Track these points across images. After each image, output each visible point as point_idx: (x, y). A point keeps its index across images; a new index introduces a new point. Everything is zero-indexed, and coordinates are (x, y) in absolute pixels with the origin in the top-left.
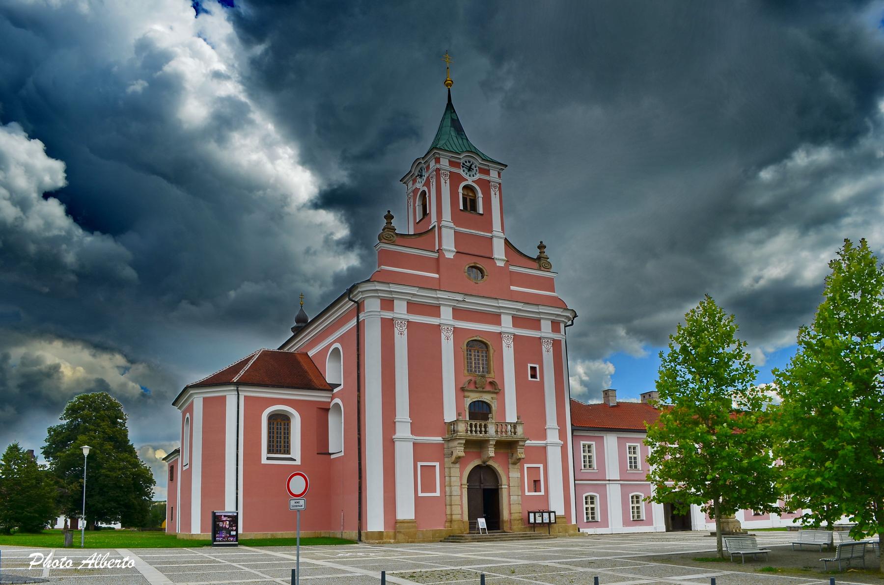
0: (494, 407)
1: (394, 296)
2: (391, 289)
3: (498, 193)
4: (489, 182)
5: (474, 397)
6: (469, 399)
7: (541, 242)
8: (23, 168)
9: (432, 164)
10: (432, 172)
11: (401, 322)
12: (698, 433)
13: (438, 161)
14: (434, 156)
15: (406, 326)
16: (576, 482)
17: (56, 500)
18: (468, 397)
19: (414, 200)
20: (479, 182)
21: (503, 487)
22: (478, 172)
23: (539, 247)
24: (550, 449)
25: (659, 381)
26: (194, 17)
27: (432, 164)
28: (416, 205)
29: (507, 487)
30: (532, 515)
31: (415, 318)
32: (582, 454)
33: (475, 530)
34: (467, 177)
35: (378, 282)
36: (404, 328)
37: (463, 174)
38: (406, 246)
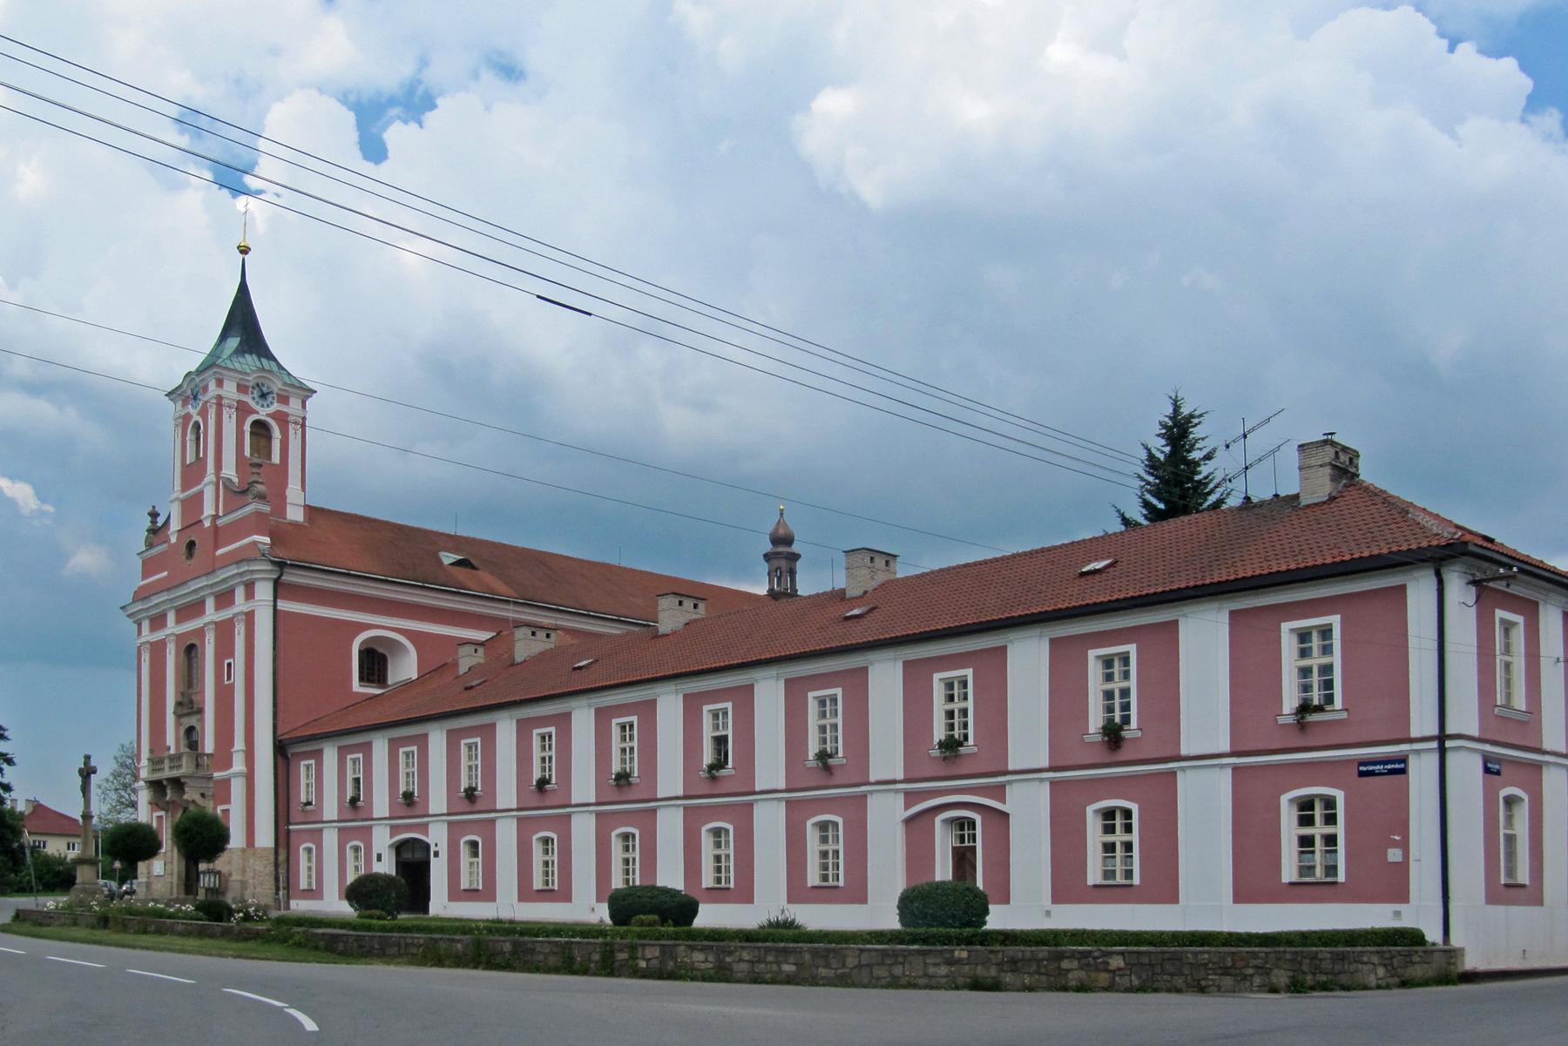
1: (231, 583)
3: (299, 432)
4: (287, 415)
7: (154, 507)
8: (1329, 467)
9: (212, 387)
10: (211, 398)
12: (251, 906)
13: (220, 383)
19: (183, 430)
20: (275, 416)
22: (275, 401)
23: (150, 514)
24: (233, 781)
25: (95, 820)
26: (1142, 441)
27: (212, 387)
28: (188, 438)
33: (969, 830)
34: (257, 408)
35: (154, 594)
37: (252, 404)
38: (1001, 438)
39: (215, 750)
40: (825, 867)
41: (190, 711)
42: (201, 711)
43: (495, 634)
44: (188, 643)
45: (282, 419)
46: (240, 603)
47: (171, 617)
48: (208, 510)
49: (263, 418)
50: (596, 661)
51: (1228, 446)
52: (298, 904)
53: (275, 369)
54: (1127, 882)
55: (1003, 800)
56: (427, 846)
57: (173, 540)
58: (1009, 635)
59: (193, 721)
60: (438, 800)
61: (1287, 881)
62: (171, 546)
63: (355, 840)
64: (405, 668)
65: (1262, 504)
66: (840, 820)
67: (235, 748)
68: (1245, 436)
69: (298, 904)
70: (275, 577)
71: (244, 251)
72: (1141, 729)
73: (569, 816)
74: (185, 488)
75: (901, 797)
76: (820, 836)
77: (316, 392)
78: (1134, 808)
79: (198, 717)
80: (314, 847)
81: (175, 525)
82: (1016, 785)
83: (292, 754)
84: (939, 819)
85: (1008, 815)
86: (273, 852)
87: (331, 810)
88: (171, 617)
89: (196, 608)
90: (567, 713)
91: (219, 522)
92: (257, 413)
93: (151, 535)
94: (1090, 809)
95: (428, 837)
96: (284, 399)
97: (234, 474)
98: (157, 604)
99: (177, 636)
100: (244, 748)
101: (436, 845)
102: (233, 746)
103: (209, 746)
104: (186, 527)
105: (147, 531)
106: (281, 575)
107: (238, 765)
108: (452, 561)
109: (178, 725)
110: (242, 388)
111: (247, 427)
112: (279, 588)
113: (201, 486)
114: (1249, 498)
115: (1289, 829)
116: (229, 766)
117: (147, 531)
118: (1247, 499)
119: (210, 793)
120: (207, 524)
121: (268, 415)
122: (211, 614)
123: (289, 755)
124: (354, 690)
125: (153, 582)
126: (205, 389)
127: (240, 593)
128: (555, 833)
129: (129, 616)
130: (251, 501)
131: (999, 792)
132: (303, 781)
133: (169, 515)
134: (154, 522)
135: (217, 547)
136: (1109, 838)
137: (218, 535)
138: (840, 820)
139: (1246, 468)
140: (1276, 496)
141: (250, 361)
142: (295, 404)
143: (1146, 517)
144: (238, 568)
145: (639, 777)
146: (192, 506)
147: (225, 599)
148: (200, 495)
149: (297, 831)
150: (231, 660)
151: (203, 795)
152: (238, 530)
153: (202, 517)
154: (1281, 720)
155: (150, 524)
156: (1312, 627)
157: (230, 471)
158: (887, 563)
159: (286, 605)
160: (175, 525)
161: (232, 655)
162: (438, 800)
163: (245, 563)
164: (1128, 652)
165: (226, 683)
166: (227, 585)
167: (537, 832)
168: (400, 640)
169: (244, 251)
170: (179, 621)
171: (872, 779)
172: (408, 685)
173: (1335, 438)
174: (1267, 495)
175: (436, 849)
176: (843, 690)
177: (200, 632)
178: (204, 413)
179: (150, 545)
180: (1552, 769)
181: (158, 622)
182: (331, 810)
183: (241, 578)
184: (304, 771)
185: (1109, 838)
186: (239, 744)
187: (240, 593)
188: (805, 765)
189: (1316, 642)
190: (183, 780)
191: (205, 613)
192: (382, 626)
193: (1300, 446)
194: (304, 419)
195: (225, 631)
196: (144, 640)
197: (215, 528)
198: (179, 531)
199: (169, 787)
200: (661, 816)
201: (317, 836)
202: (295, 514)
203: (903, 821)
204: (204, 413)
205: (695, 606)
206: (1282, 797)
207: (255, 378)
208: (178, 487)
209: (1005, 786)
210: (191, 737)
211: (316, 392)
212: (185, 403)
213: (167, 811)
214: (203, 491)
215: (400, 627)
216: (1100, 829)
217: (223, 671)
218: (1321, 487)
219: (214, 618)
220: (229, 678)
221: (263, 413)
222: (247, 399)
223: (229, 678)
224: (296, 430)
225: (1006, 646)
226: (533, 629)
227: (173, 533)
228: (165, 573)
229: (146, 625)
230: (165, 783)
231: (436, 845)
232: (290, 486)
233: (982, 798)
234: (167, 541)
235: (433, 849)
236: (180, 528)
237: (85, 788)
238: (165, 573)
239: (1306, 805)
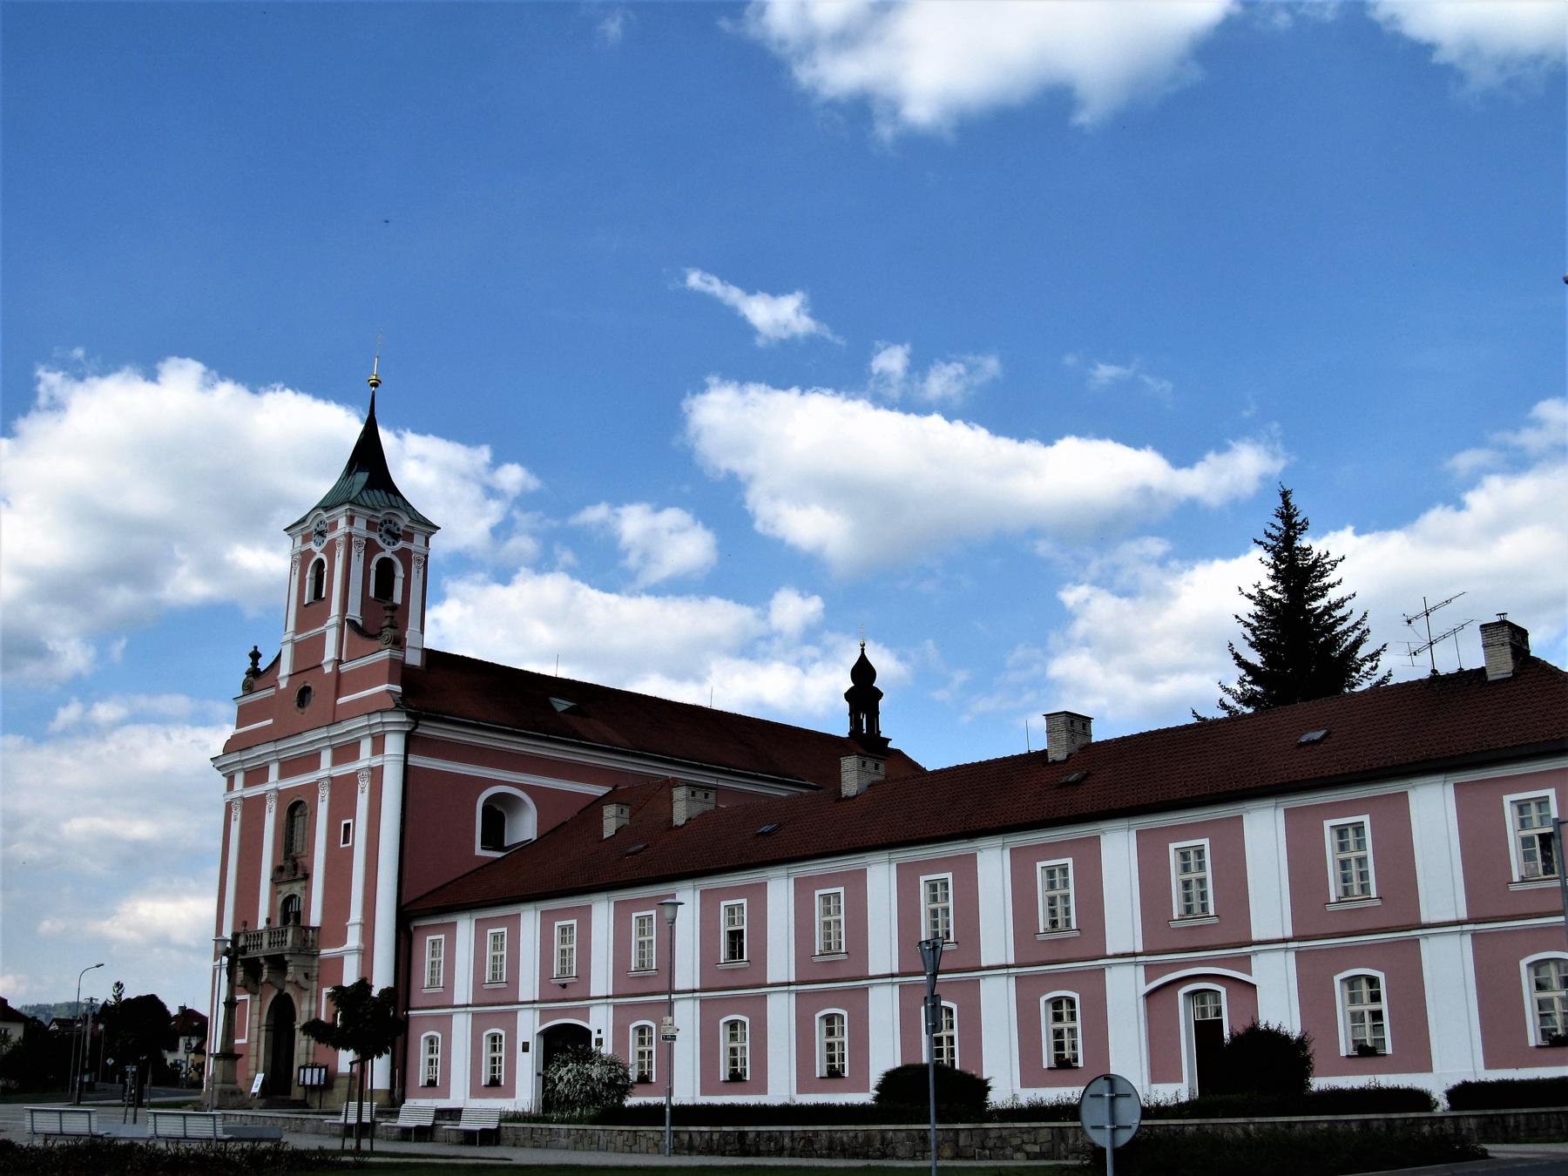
3: (421, 571)
7: (256, 647)
20: (399, 553)
23: (251, 655)
24: (346, 959)
34: (383, 545)
41: (291, 878)
42: (307, 877)
43: (611, 789)
44: (295, 800)
45: (405, 555)
46: (366, 758)
47: (274, 770)
48: (330, 653)
49: (388, 556)
50: (780, 825)
51: (1409, 622)
53: (401, 505)
55: (1250, 973)
56: (589, 1033)
57: (283, 685)
58: (1246, 805)
59: (296, 889)
60: (601, 980)
62: (278, 691)
63: (499, 1028)
64: (525, 827)
65: (1449, 677)
66: (747, 1020)
67: (351, 921)
68: (1427, 615)
72: (1381, 898)
73: (764, 996)
74: (299, 629)
75: (1141, 970)
77: (439, 528)
78: (1381, 975)
79: (303, 884)
80: (439, 1036)
81: (285, 669)
82: (1114, 969)
83: (415, 927)
84: (1181, 993)
85: (1255, 986)
87: (463, 992)
88: (274, 770)
89: (310, 761)
90: (763, 883)
91: (343, 668)
92: (384, 550)
93: (251, 678)
94: (1337, 979)
95: (588, 1022)
96: (409, 537)
97: (358, 615)
98: (258, 756)
101: (599, 1032)
102: (348, 918)
103: (315, 918)
105: (246, 674)
106: (416, 727)
107: (354, 939)
108: (566, 707)
109: (274, 893)
110: (370, 526)
111: (373, 567)
112: (412, 743)
113: (323, 628)
114: (1436, 671)
118: (1434, 671)
120: (328, 669)
121: (384, 550)
122: (326, 767)
123: (412, 929)
124: (477, 854)
125: (257, 729)
126: (334, 526)
127: (366, 747)
128: (654, 1022)
129: (218, 769)
130: (383, 647)
131: (1244, 963)
132: (428, 959)
133: (280, 655)
134: (255, 663)
135: (337, 696)
137: (340, 683)
138: (845, 1013)
139: (1431, 643)
140: (1461, 669)
141: (379, 495)
142: (419, 540)
143: (1262, 663)
145: (847, 953)
146: (308, 652)
147: (347, 752)
148: (323, 636)
149: (421, 1017)
150: (350, 821)
151: (306, 976)
152: (364, 678)
153: (323, 662)
155: (250, 666)
157: (354, 612)
158: (1084, 725)
159: (417, 760)
160: (285, 669)
161: (352, 814)
162: (601, 980)
165: (342, 846)
167: (1045, 993)
168: (517, 795)
170: (283, 775)
171: (1109, 952)
172: (528, 846)
173: (1509, 618)
174: (1453, 669)
175: (599, 1036)
177: (313, 788)
178: (330, 550)
179: (248, 688)
180: (595, 1007)
181: (257, 775)
182: (463, 992)
184: (428, 944)
186: (356, 915)
187: (366, 747)
188: (1035, 938)
191: (319, 767)
192: (505, 781)
193: (1482, 626)
194: (426, 556)
195: (343, 790)
196: (234, 795)
197: (338, 675)
198: (290, 676)
199: (266, 966)
200: (874, 994)
201: (445, 1024)
202: (414, 659)
203: (1144, 996)
204: (330, 550)
205: (877, 767)
207: (384, 515)
208: (291, 627)
209: (1250, 957)
210: (291, 912)
211: (439, 528)
212: (306, 539)
213: (253, 993)
214: (325, 633)
215: (463, 773)
217: (341, 833)
218: (1504, 666)
219: (332, 773)
220: (346, 841)
221: (388, 553)
222: (375, 536)
223: (346, 841)
224: (419, 568)
225: (1242, 816)
226: (693, 789)
227: (283, 678)
228: (270, 722)
229: (239, 779)
230: (262, 961)
231: (599, 1032)
232: (409, 628)
233: (1230, 971)
234: (275, 685)
235: (595, 1036)
237: (231, 970)
238: (270, 722)
239: (1056, 1003)
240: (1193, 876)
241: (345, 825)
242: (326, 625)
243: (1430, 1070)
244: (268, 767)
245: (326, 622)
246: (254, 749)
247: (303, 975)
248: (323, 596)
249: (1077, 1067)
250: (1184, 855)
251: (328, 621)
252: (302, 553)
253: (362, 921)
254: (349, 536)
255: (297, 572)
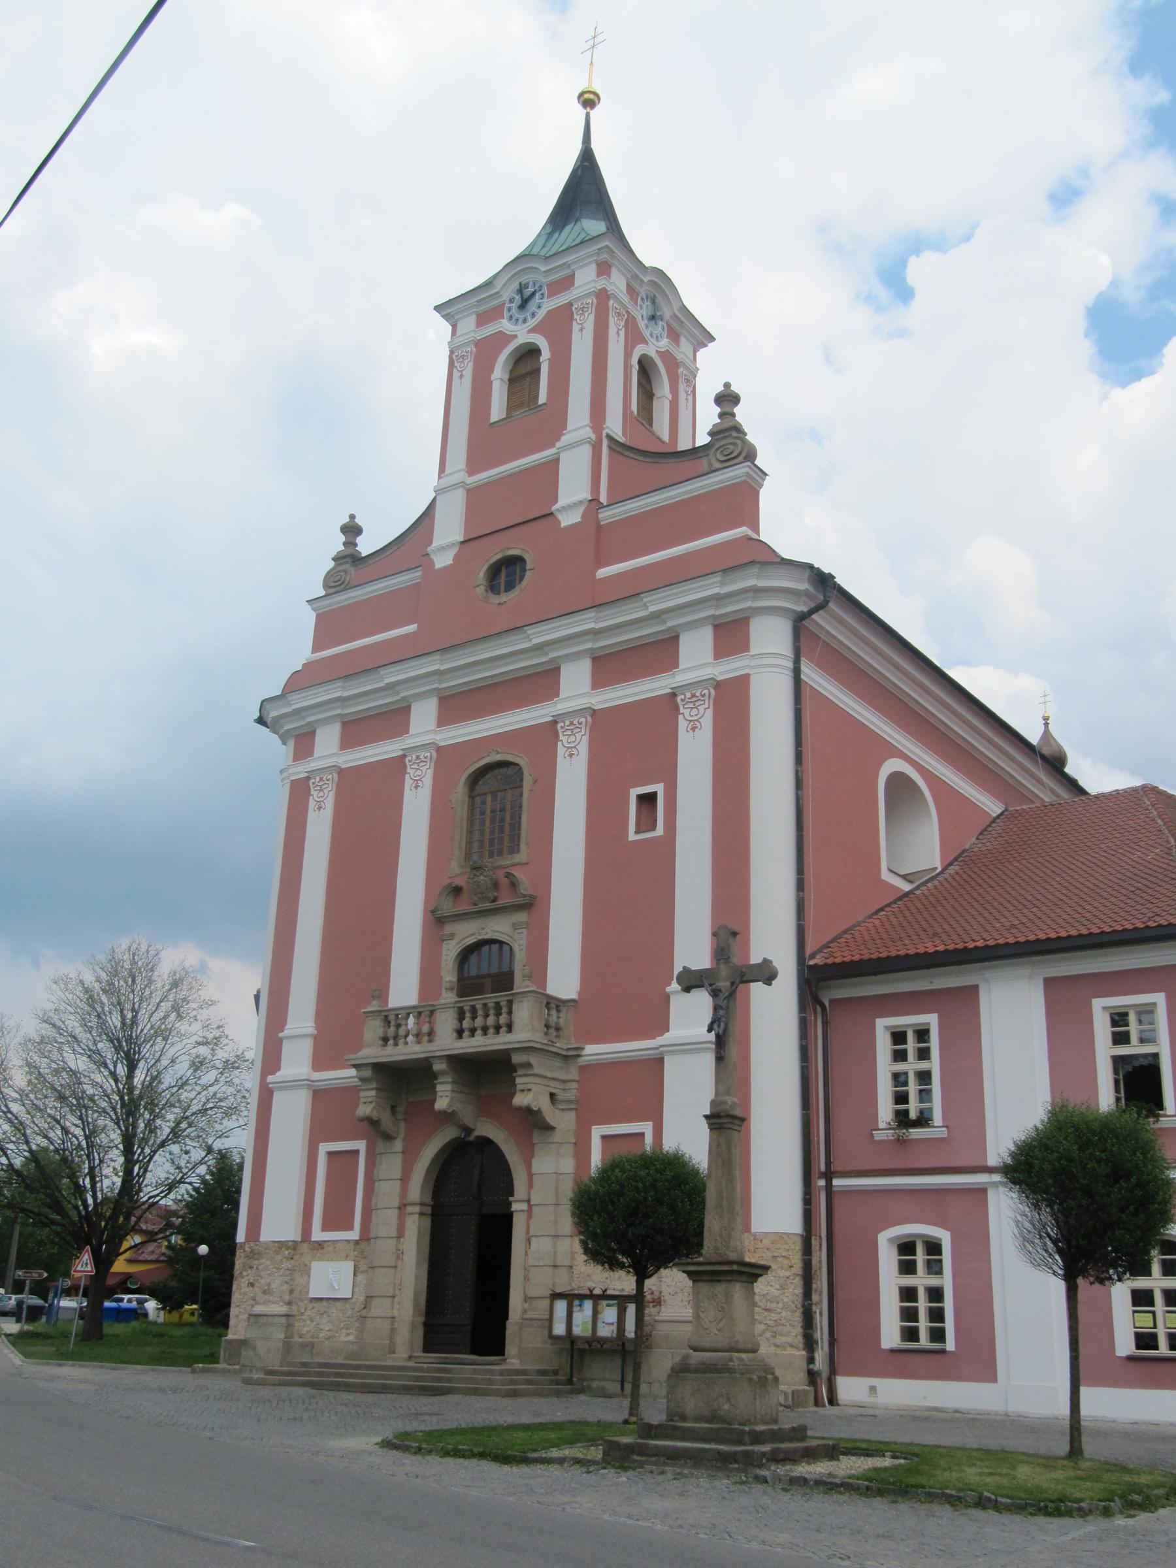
0: (520, 945)
1: (309, 719)
2: (294, 707)
5: (467, 932)
6: (454, 942)
11: (572, 723)
14: (598, 254)
15: (583, 730)
16: (836, 1182)
17: (623, 1344)
18: (452, 936)
21: (417, 1209)
24: (672, 1069)
29: (524, 1206)
30: (561, 1307)
31: (462, 731)
32: (934, 1064)
36: (424, 769)
39: (580, 994)
40: (909, 1315)
45: (672, 363)
52: (873, 1389)
54: (936, 1346)
61: (1124, 1355)
69: (873, 1389)
70: (803, 608)
71: (589, 101)
72: (947, 1127)
76: (900, 1262)
78: (945, 1237)
83: (832, 1001)
86: (798, 1246)
99: (439, 750)
100: (314, 1025)
104: (469, 540)
105: (334, 559)
115: (890, 1280)
116: (662, 1025)
117: (334, 559)
119: (572, 1095)
134: (350, 544)
136: (909, 1281)
144: (722, 584)
153: (554, 508)
154: (879, 1136)
156: (908, 1026)
163: (755, 570)
164: (1154, 1004)
166: (662, 628)
169: (589, 101)
170: (446, 718)
176: (940, 1017)
183: (717, 607)
185: (909, 1281)
188: (872, 1135)
189: (911, 1045)
190: (516, 1059)
196: (313, 764)
198: (462, 543)
206: (949, 1233)
214: (557, 460)
216: (895, 1267)
228: (413, 628)
229: (327, 741)
230: (438, 1066)
236: (462, 540)
238: (413, 628)
239: (906, 1247)
240: (912, 1066)
241: (641, 798)
242: (559, 444)
243: (993, 1378)
244: (558, 669)
245: (559, 439)
246: (383, 672)
247: (548, 1098)
248: (542, 398)
249: (943, 1351)
250: (899, 1037)
251: (563, 438)
252: (478, 344)
253: (316, 1032)
254: (603, 296)
255: (468, 373)
